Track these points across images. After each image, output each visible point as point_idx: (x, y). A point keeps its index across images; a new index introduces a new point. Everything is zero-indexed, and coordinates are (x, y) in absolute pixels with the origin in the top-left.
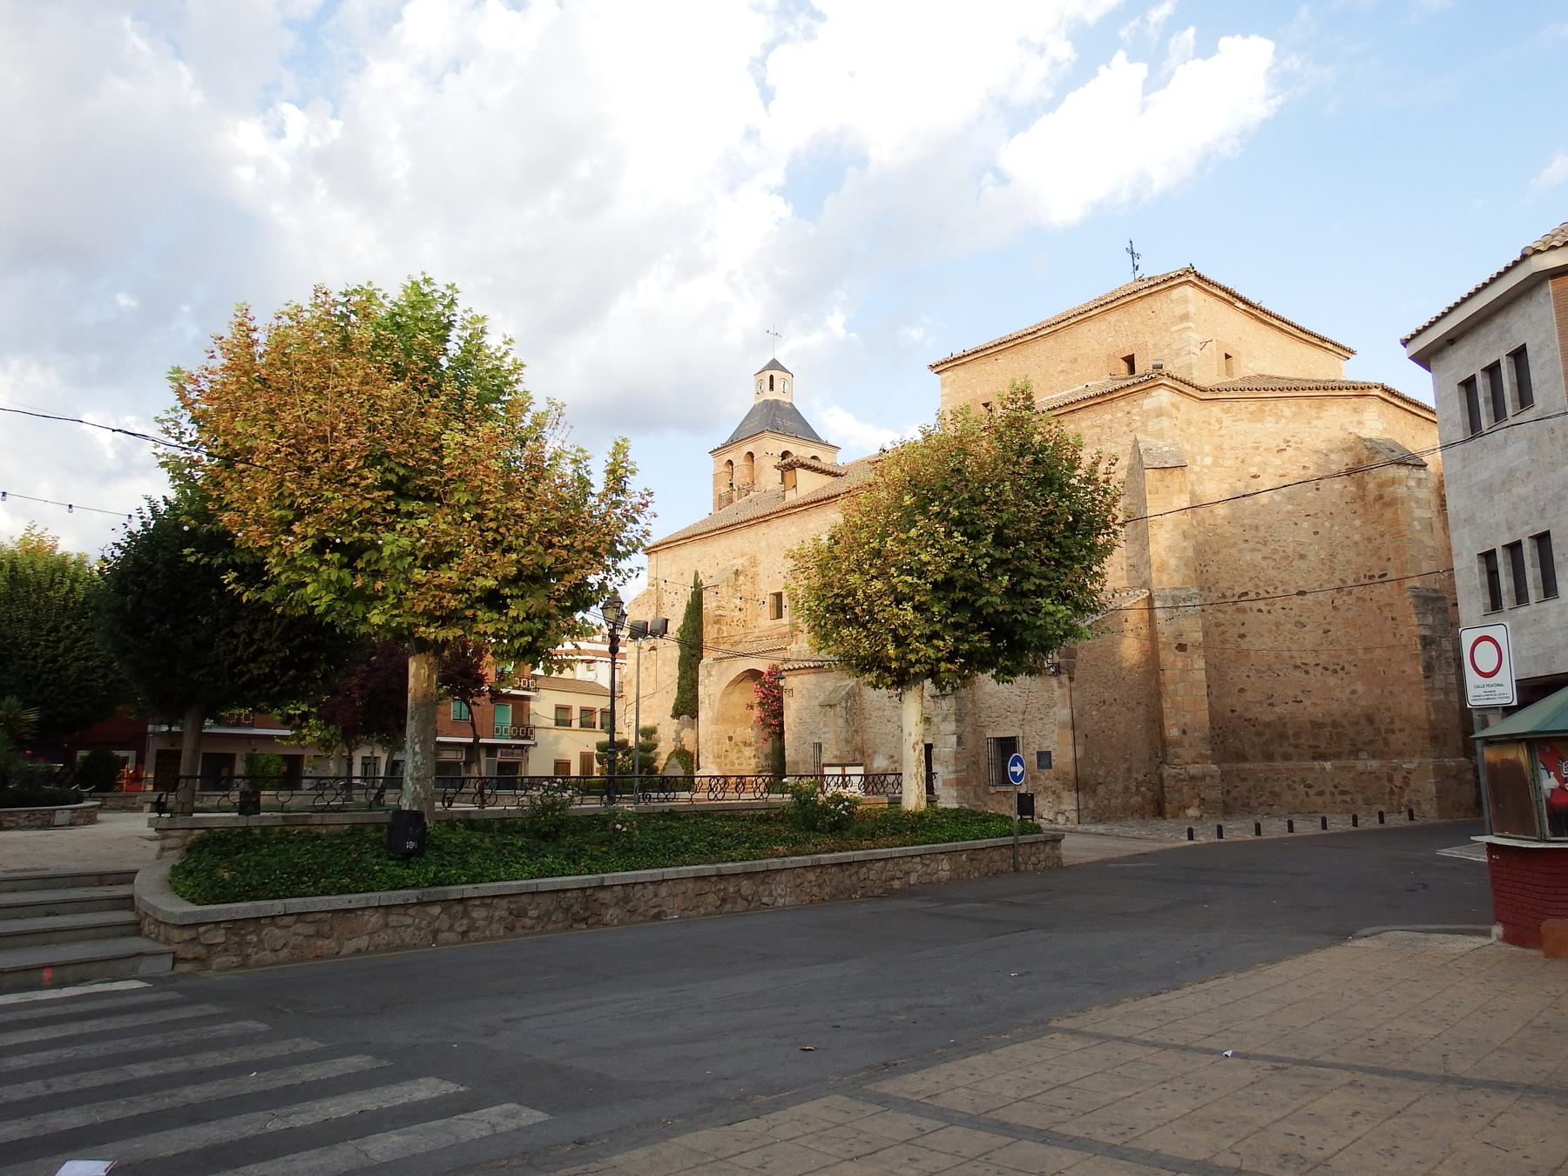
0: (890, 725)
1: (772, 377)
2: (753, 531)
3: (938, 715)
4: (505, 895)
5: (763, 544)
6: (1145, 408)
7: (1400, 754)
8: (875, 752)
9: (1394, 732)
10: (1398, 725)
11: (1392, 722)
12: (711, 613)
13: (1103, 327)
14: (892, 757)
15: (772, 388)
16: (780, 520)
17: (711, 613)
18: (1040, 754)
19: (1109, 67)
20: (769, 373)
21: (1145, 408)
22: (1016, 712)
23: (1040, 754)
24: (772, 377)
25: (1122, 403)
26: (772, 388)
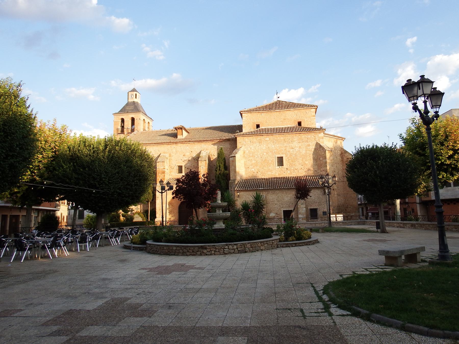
0: (276, 205)
1: (136, 94)
2: (169, 146)
3: (300, 203)
4: (455, 237)
5: (174, 150)
6: (319, 136)
7: (349, 212)
8: (271, 212)
9: (348, 208)
10: (349, 206)
11: (348, 206)
12: (161, 170)
13: (293, 113)
14: (277, 213)
15: (136, 98)
16: (182, 144)
17: (161, 170)
18: (323, 212)
19: (436, 88)
20: (135, 93)
21: (319, 136)
22: (317, 203)
23: (323, 212)
24: (136, 94)
25: (313, 134)
26: (136, 98)
